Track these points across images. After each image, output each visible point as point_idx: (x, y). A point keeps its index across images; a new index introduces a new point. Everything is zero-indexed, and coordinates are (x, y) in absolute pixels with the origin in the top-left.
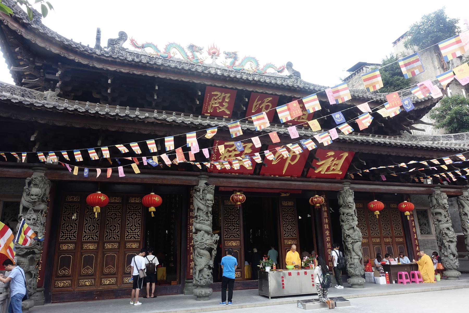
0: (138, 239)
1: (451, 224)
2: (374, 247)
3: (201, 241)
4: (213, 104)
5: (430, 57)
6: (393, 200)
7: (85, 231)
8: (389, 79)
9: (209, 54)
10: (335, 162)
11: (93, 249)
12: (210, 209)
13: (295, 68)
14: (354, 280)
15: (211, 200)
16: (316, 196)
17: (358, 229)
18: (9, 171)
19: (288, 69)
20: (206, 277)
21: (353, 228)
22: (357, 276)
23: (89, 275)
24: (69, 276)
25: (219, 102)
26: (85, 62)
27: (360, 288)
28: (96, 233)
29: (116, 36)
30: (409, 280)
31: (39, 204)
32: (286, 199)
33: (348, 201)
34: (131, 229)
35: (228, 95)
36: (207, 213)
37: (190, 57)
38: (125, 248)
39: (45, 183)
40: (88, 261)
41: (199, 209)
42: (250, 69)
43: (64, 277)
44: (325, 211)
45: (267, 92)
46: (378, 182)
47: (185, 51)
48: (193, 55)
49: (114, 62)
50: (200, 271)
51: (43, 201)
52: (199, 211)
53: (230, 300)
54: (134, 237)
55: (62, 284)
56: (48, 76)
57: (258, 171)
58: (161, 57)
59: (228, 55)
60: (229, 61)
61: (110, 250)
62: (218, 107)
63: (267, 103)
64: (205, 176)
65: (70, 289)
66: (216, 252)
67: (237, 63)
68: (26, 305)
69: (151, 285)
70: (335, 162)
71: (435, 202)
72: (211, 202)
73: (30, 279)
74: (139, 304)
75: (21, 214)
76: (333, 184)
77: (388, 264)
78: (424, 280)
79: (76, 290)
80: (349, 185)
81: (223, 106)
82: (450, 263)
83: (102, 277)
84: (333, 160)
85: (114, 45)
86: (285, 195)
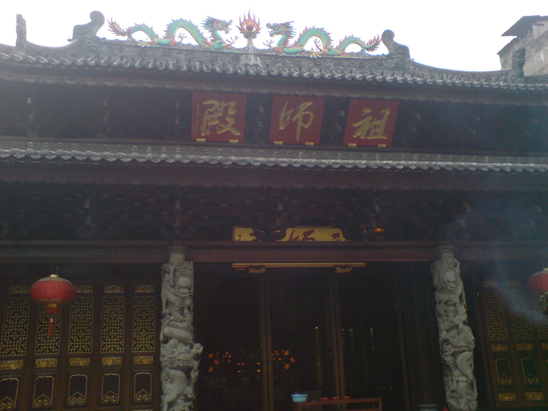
3: (171, 356)
4: (208, 121)
9: (241, 30)
11: (16, 369)
12: (188, 302)
13: (398, 39)
15: (186, 288)
21: (457, 327)
25: (219, 118)
28: (22, 343)
29: (86, 20)
34: (77, 336)
35: (233, 104)
37: (209, 41)
48: (213, 35)
54: (82, 348)
59: (275, 29)
60: (278, 38)
63: (305, 111)
66: (197, 374)
67: (291, 42)
84: (371, 121)
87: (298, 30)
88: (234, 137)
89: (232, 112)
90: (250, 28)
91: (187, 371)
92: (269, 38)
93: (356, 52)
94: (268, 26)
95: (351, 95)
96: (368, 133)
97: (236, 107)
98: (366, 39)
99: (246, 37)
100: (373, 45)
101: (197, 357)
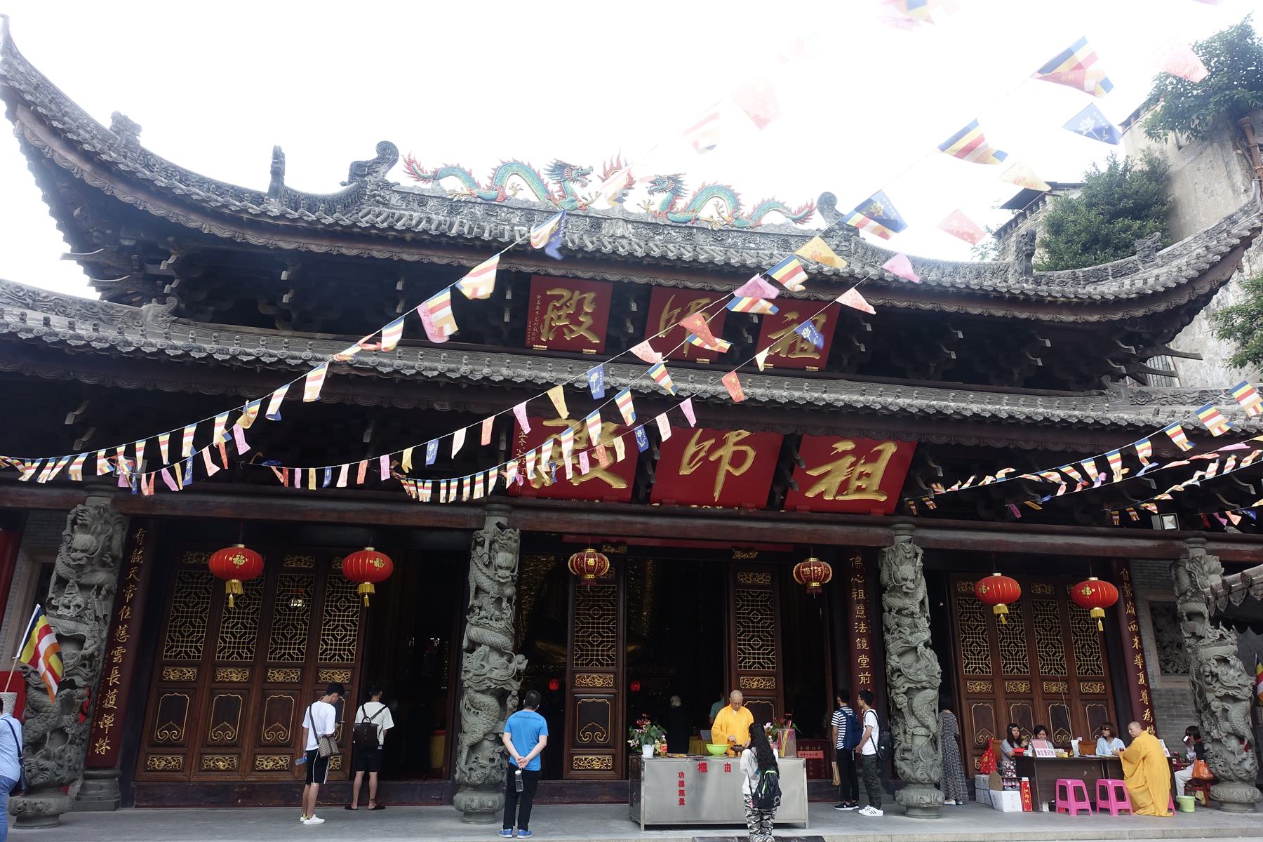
0: (351, 659)
1: (1235, 648)
2: (1008, 706)
5: (1220, 162)
6: (1049, 578)
7: (222, 638)
8: (1099, 229)
10: (860, 469)
12: (509, 591)
14: (913, 795)
15: (507, 568)
16: (812, 560)
17: (929, 653)
18: (33, 494)
19: (822, 212)
20: (485, 762)
21: (916, 648)
22: (918, 783)
23: (227, 746)
24: (181, 746)
25: (569, 316)
27: (928, 817)
29: (370, 155)
30: (1086, 805)
31: (93, 571)
32: (748, 566)
33: (899, 575)
35: (590, 296)
36: (499, 601)
37: (556, 196)
38: (317, 683)
39: (106, 522)
40: (226, 712)
41: (479, 590)
42: (716, 216)
43: (169, 746)
44: (858, 601)
45: (689, 284)
46: (999, 524)
47: (542, 181)
48: (562, 189)
49: (292, 229)
50: (474, 747)
51: (104, 565)
52: (481, 595)
53: (524, 826)
55: (163, 763)
57: (642, 494)
58: (479, 200)
59: (657, 185)
60: (660, 199)
61: (279, 685)
62: (566, 326)
64: (503, 507)
65: (180, 776)
67: (680, 204)
68: (49, 806)
69: (366, 778)
70: (860, 469)
71: (1186, 581)
72: (508, 573)
73: (61, 747)
74: (316, 820)
75: (50, 595)
76: (862, 529)
77: (1030, 755)
78: (1136, 808)
79: (195, 779)
80: (911, 530)
81: (580, 324)
82: (1226, 763)
83: (257, 750)
84: (853, 464)
85: (364, 176)
86: (745, 556)
98: (795, 205)
101: (518, 675)
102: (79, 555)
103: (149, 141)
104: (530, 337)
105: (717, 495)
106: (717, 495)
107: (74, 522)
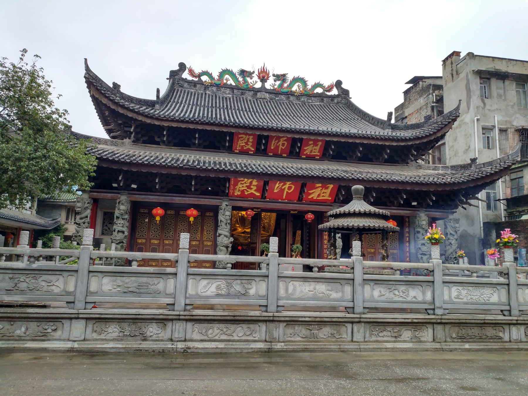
9: (259, 77)
12: (229, 221)
25: (247, 186)
26: (148, 121)
29: (177, 68)
36: (226, 224)
51: (127, 213)
56: (126, 129)
62: (245, 190)
67: (285, 85)
70: (323, 191)
71: (417, 222)
75: (115, 221)
87: (290, 77)
88: (252, 151)
89: (251, 141)
90: (264, 77)
91: (227, 247)
92: (273, 82)
93: (320, 92)
94: (274, 75)
95: (303, 137)
96: (311, 151)
97: (252, 138)
98: (326, 85)
99: (261, 81)
100: (330, 89)
101: (231, 243)
102: (122, 211)
103: (123, 90)
104: (234, 148)
105: (284, 197)
106: (284, 197)
107: (119, 203)
